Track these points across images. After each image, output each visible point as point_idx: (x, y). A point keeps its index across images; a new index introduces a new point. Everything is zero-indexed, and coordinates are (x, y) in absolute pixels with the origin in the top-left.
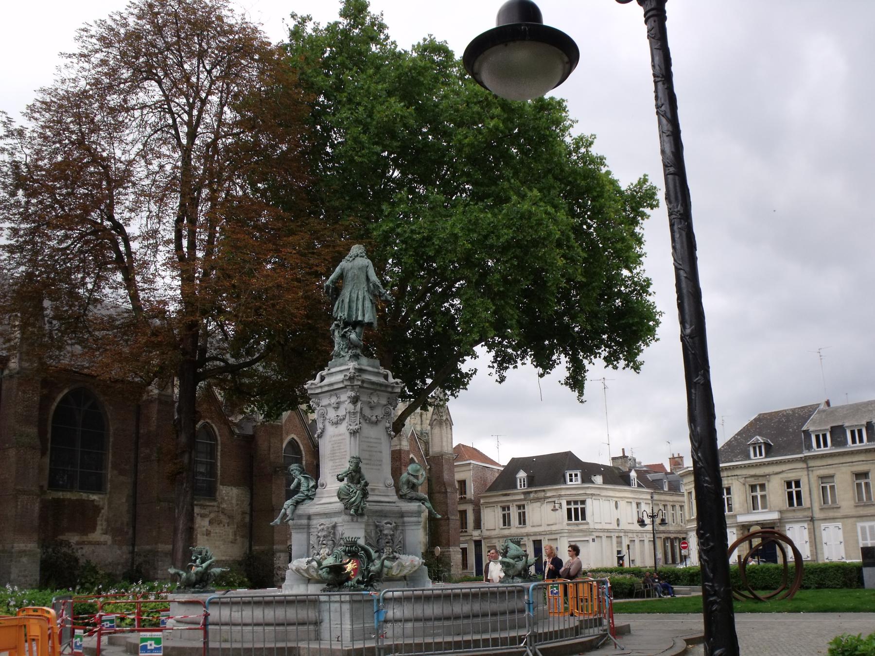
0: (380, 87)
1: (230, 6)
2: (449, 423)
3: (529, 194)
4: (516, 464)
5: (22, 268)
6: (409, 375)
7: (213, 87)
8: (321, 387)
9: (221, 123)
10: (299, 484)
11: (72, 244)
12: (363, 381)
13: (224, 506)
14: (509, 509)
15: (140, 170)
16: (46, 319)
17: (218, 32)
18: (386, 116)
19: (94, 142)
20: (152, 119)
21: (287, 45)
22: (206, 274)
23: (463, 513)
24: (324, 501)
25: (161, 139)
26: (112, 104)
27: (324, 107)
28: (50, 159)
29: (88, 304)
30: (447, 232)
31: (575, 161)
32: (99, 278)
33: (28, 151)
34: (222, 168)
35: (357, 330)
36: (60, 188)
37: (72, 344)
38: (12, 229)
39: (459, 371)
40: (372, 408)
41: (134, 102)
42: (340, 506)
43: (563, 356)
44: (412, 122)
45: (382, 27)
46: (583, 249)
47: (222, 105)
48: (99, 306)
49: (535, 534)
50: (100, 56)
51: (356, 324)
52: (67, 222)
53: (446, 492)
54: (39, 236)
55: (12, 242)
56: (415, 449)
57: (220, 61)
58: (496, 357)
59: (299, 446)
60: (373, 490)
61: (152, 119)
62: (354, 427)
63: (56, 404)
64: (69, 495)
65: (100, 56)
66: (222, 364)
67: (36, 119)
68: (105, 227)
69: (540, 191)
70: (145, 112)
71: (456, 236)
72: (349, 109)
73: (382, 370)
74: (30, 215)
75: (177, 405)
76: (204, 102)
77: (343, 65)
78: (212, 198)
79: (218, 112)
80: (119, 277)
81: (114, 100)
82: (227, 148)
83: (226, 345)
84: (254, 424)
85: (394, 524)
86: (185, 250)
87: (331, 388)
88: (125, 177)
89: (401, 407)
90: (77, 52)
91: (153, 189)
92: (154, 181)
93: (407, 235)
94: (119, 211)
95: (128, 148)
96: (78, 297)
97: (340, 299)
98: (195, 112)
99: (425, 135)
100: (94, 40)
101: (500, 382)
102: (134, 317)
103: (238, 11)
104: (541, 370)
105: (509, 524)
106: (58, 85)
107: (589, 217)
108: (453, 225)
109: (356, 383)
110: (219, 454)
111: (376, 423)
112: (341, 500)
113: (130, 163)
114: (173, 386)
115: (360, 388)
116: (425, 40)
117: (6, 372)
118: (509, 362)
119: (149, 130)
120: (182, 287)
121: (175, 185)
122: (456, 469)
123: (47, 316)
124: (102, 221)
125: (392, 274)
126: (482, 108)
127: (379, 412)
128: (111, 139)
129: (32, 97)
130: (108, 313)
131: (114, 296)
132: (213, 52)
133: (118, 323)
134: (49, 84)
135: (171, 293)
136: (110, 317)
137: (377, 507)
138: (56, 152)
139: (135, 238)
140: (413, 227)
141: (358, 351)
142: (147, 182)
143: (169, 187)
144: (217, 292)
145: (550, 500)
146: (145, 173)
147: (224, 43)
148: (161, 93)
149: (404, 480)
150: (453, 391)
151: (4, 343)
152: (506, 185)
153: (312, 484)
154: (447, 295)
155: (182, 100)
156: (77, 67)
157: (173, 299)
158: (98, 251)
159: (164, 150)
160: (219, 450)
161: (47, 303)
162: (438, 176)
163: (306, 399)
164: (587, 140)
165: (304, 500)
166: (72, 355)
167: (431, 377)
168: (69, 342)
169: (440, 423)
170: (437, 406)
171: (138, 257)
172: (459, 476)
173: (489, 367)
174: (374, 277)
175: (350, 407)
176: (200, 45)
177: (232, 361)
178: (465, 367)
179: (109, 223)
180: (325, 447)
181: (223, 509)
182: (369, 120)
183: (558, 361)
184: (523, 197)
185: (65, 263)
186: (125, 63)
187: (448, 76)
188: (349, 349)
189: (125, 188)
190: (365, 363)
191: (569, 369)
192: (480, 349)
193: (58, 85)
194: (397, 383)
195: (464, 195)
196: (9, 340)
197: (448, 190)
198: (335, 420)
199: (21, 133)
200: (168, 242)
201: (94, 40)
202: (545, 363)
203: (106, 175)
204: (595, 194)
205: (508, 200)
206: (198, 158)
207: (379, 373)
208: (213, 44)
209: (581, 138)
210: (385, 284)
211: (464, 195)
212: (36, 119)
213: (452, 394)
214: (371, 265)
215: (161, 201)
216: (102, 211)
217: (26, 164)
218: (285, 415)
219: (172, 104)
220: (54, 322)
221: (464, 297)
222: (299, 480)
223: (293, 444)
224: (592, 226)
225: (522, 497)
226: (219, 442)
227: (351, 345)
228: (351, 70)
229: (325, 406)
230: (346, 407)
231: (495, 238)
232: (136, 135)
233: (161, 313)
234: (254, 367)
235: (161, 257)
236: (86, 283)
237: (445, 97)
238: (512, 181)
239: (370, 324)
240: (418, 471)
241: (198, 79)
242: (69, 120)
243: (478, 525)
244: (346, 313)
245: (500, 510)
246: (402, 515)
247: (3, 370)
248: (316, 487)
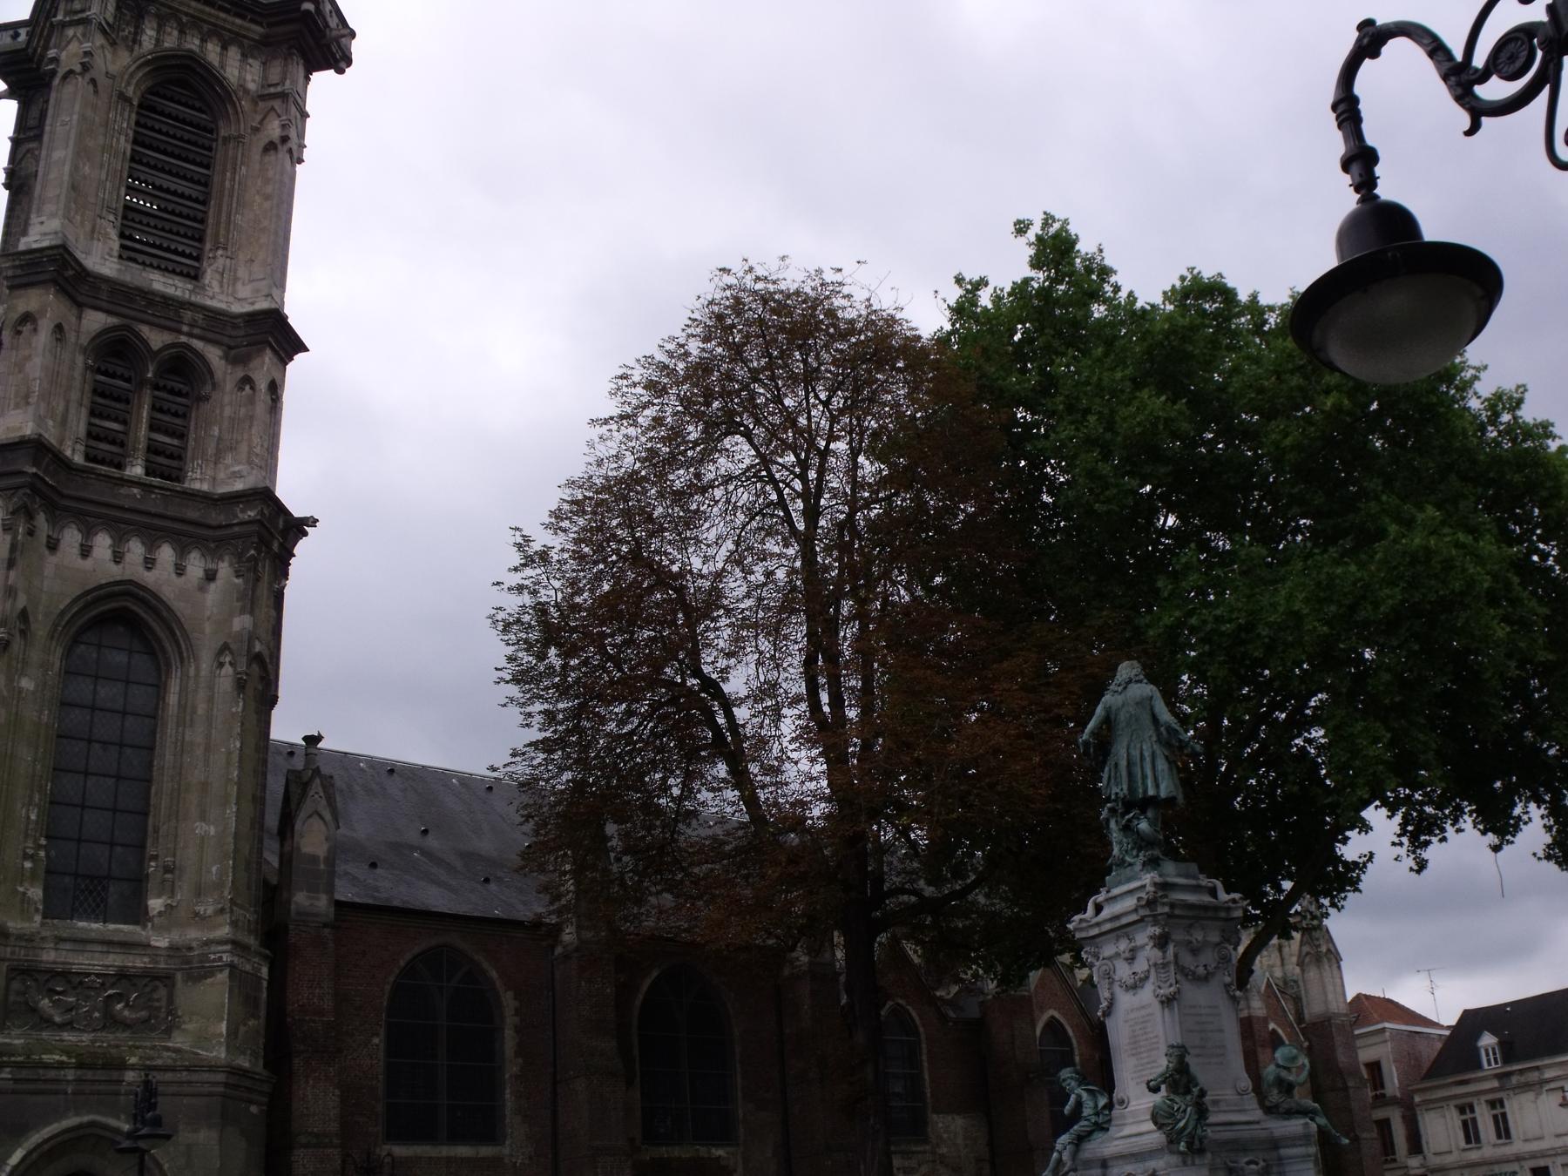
0: (1119, 375)
1: (846, 290)
2: (1334, 957)
3: (1420, 517)
4: (1473, 1021)
5: (567, 776)
6: (1247, 880)
7: (836, 427)
8: (1098, 924)
9: (856, 484)
10: (1079, 1104)
11: (640, 724)
12: (1172, 906)
13: (943, 1150)
14: (1472, 1111)
15: (735, 586)
16: (612, 855)
17: (831, 336)
18: (1139, 424)
19: (657, 552)
20: (743, 497)
21: (950, 333)
22: (867, 746)
23: (1384, 1126)
24: (1126, 1131)
25: (762, 529)
26: (678, 485)
27: (1027, 426)
28: (592, 591)
29: (676, 821)
30: (1281, 609)
31: (1494, 440)
32: (689, 777)
33: (557, 584)
34: (869, 561)
35: (1150, 814)
36: (612, 635)
37: (658, 893)
38: (546, 712)
39: (1339, 859)
40: (1195, 952)
41: (711, 476)
42: (1157, 1138)
43: (1532, 806)
44: (1185, 426)
45: (1105, 272)
46: (1540, 599)
47: (854, 453)
48: (694, 822)
49: (1534, 1156)
50: (650, 412)
51: (1146, 804)
52: (627, 690)
53: (1346, 1089)
54: (588, 719)
55: (548, 734)
56: (1276, 1012)
57: (842, 383)
58: (1403, 826)
59: (1065, 1031)
60: (1215, 1103)
61: (743, 497)
62: (1167, 991)
63: (641, 997)
64: (676, 1152)
65: (650, 412)
66: (913, 899)
67: (565, 531)
68: (690, 689)
69: (1438, 506)
70: (731, 488)
71: (1297, 616)
72: (1072, 423)
73: (1204, 881)
74: (570, 686)
75: (842, 978)
76: (825, 454)
77: (1048, 349)
78: (861, 615)
79: (852, 466)
80: (721, 770)
81: (679, 478)
82: (872, 525)
83: (915, 865)
84: (981, 998)
85: (1262, 1164)
86: (826, 709)
87: (1117, 924)
88: (714, 598)
89: (1246, 939)
90: (615, 412)
91: (761, 614)
92: (760, 599)
93: (1209, 627)
94: (709, 660)
95: (711, 551)
96: (659, 811)
97: (1111, 762)
98: (812, 475)
99: (1211, 444)
100: (639, 390)
101: (1418, 872)
102: (755, 834)
103: (860, 296)
104: (1491, 838)
105: (1478, 1140)
106: (593, 470)
107: (1541, 539)
108: (1290, 597)
109: (1160, 910)
110: (924, 1058)
111: (1206, 979)
112: (1160, 1126)
113: (719, 575)
114: (832, 946)
115: (1169, 919)
116: (1183, 279)
117: (559, 950)
118: (1431, 833)
119: (741, 518)
120: (830, 774)
121: (793, 600)
122: (1359, 1043)
123: (613, 849)
124: (684, 681)
125: (1193, 700)
126: (1306, 378)
127: (1209, 957)
128: (682, 545)
129: (554, 497)
130: (710, 832)
131: (718, 802)
132: (827, 371)
133: (727, 848)
134: (578, 471)
135: (812, 785)
136: (714, 838)
137: (1227, 1135)
138: (599, 577)
139: (742, 701)
140: (1218, 612)
141: (1157, 852)
142: (749, 603)
143: (787, 608)
144: (891, 775)
145: (1552, 1085)
146: (744, 589)
147: (842, 351)
148: (753, 452)
149: (1271, 1078)
150: (1333, 897)
151: (551, 903)
152: (1374, 507)
153: (1102, 1102)
154: (1300, 723)
155: (790, 458)
156: (618, 437)
157: (818, 796)
158: (681, 730)
159: (772, 546)
160: (925, 1051)
161: (611, 829)
162: (1247, 514)
163: (1076, 947)
164: (1511, 398)
165: (1090, 1133)
166: (660, 909)
167: (1290, 877)
168: (653, 889)
169: (1318, 959)
170: (1307, 931)
171: (749, 731)
172: (1366, 1055)
173: (1394, 844)
174: (1165, 716)
175: (1157, 953)
176: (805, 361)
177: (929, 891)
178: (1352, 848)
179: (695, 682)
180: (1119, 1032)
181: (942, 1156)
182: (1108, 436)
183: (1525, 817)
184: (1408, 524)
185: (632, 759)
186: (692, 416)
187: (1236, 334)
188: (1140, 850)
189: (715, 620)
190: (1171, 871)
191: (1548, 828)
192: (1374, 814)
193: (593, 470)
194: (1234, 901)
195: (1299, 538)
196: (558, 897)
197: (1268, 533)
198: (1130, 982)
199: (544, 556)
200: (796, 700)
201: (639, 390)
202: (1500, 825)
203: (682, 601)
204: (1544, 494)
205: (1381, 534)
206: (828, 550)
207: (1199, 886)
208: (825, 356)
209: (1498, 396)
210: (1184, 720)
211: (1299, 538)
212: (565, 531)
213: (1333, 905)
214: (1158, 694)
215: (775, 631)
216: (681, 662)
217: (557, 605)
218: (1034, 976)
219: (774, 468)
220: (626, 859)
221: (1331, 724)
222: (1079, 1096)
223: (1053, 1026)
224: (1549, 554)
225: (1495, 1084)
226: (923, 1037)
227: (1142, 843)
228: (1064, 354)
229: (1110, 958)
230: (1149, 954)
231: (1369, 608)
232: (721, 528)
233: (798, 823)
234: (970, 898)
235: (788, 727)
236: (671, 787)
237: (1236, 370)
238: (1384, 498)
239: (1171, 801)
240: (1294, 1059)
241: (809, 418)
242: (614, 523)
243: (1416, 1146)
244: (1125, 787)
245: (1455, 1113)
246: (1275, 1144)
247: (553, 948)
248: (1110, 1106)
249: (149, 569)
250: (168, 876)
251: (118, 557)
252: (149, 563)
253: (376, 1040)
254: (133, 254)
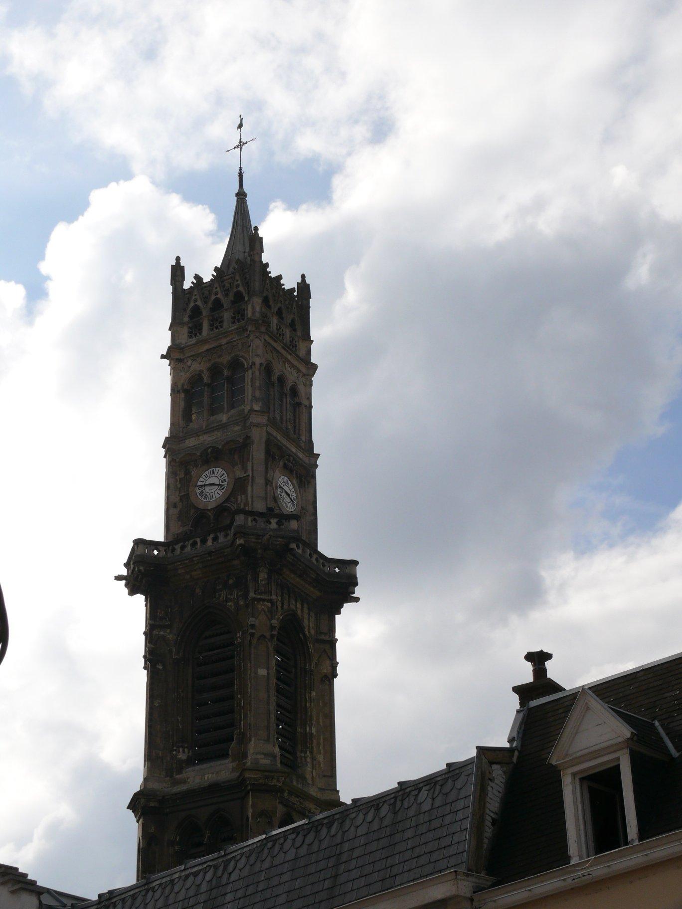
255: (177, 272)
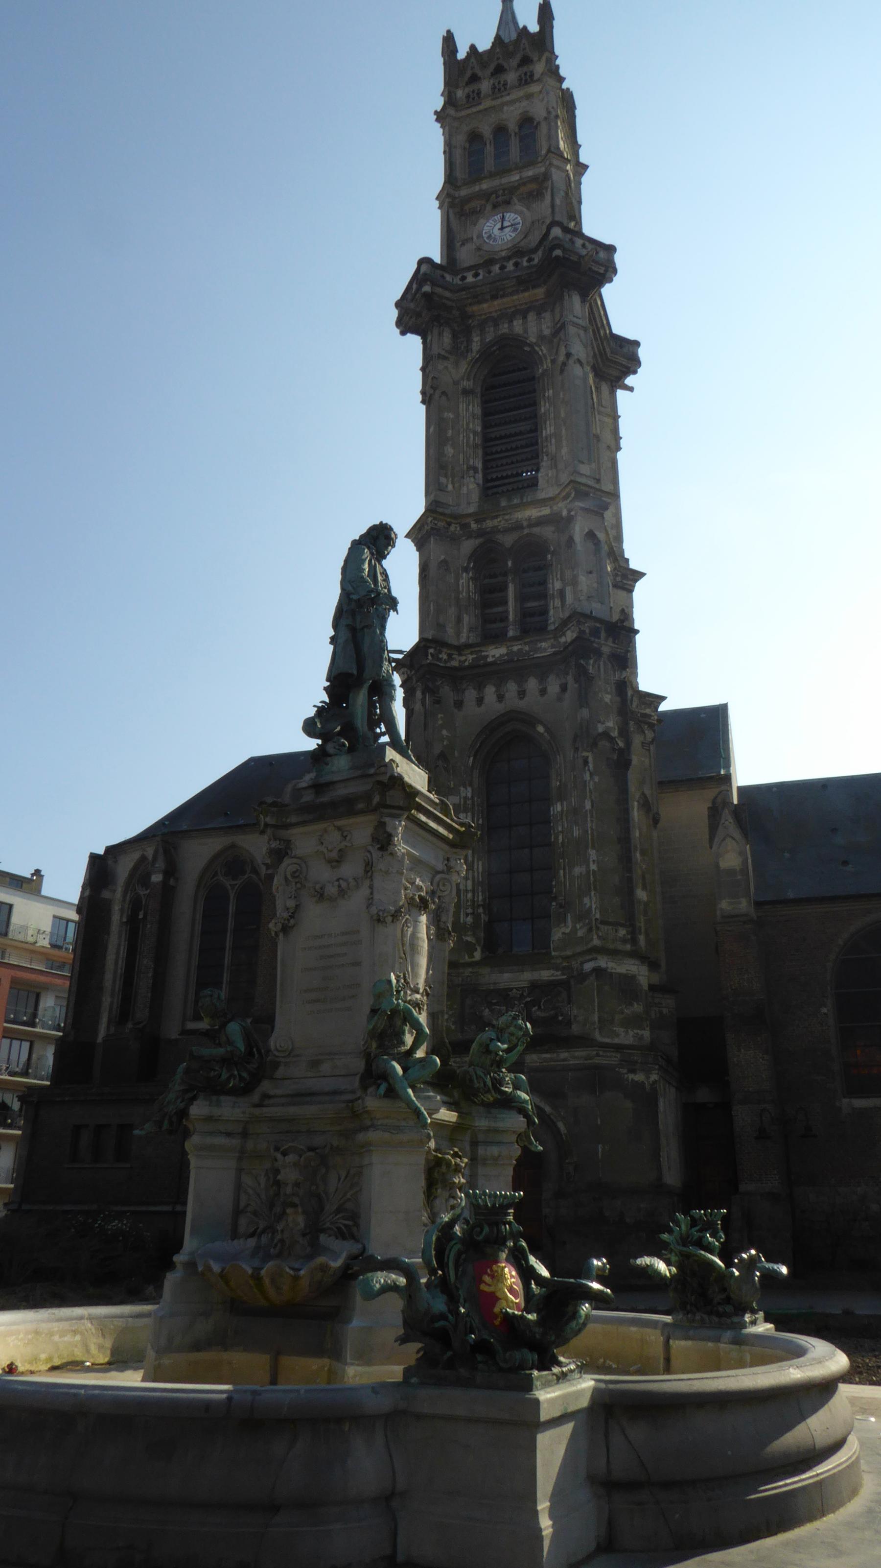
180: (131, 865)
249: (521, 699)
250: (562, 910)
251: (501, 698)
252: (522, 694)
253: (824, 1010)
254: (495, 490)
255: (449, 42)
